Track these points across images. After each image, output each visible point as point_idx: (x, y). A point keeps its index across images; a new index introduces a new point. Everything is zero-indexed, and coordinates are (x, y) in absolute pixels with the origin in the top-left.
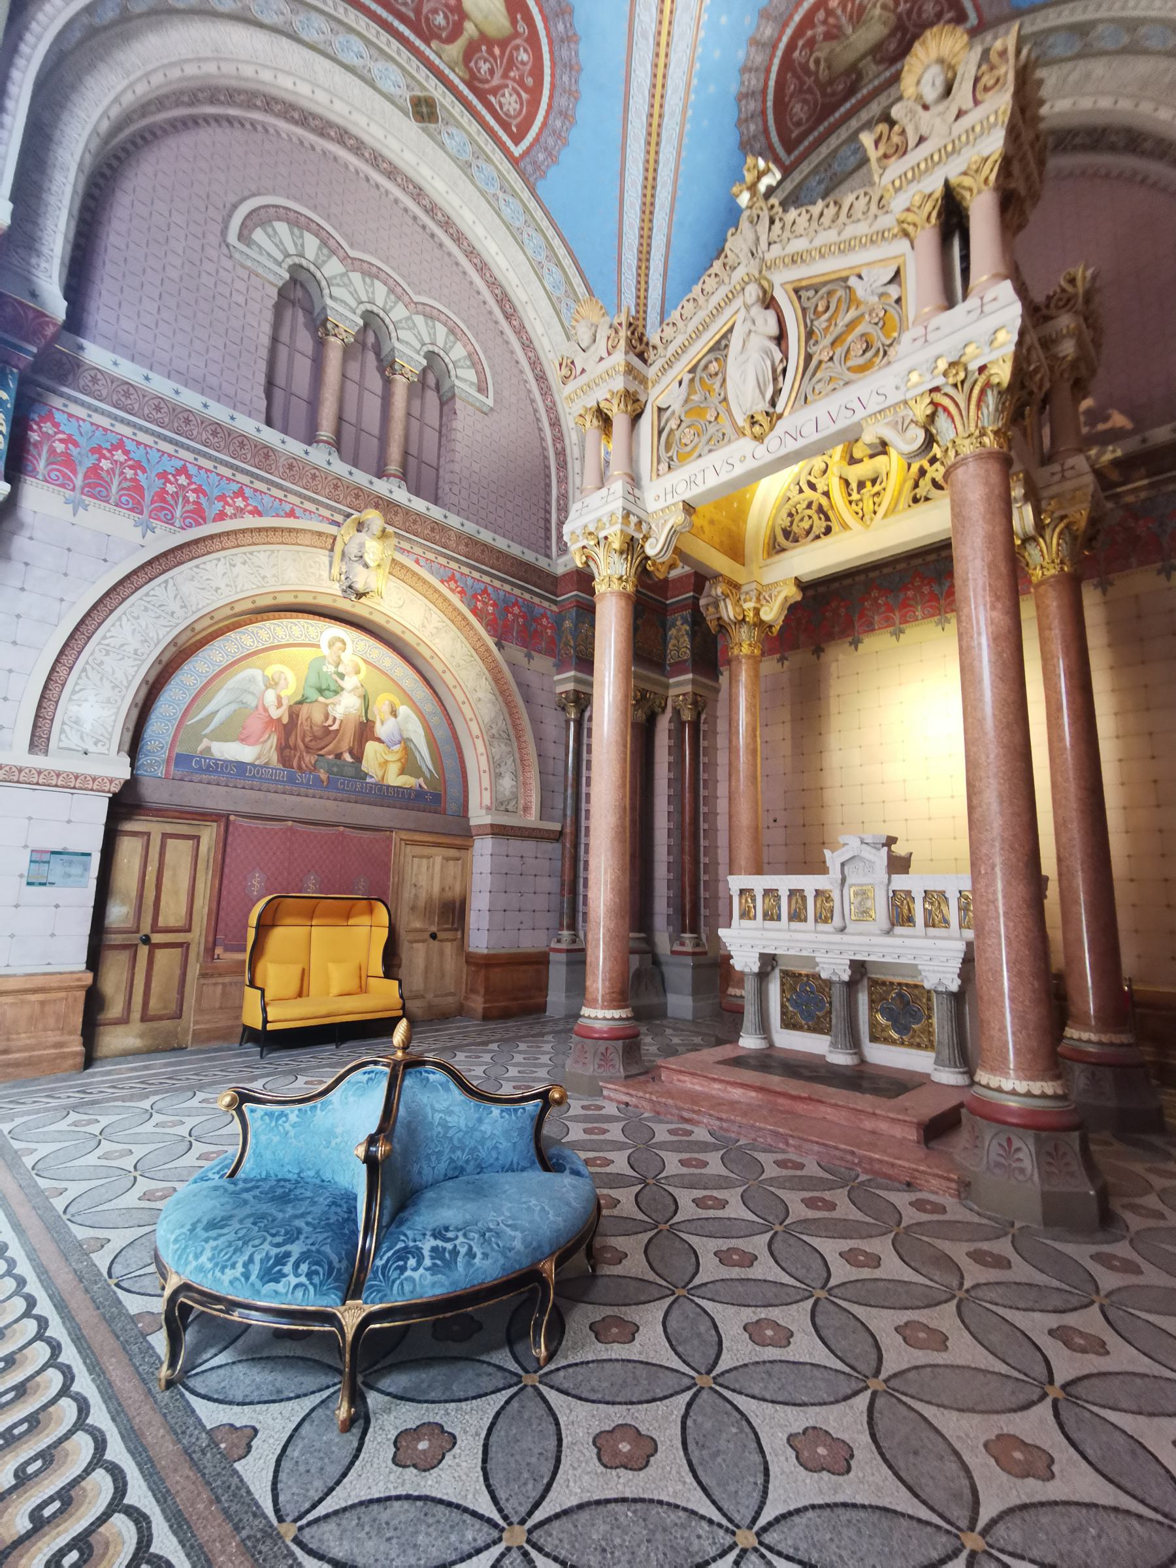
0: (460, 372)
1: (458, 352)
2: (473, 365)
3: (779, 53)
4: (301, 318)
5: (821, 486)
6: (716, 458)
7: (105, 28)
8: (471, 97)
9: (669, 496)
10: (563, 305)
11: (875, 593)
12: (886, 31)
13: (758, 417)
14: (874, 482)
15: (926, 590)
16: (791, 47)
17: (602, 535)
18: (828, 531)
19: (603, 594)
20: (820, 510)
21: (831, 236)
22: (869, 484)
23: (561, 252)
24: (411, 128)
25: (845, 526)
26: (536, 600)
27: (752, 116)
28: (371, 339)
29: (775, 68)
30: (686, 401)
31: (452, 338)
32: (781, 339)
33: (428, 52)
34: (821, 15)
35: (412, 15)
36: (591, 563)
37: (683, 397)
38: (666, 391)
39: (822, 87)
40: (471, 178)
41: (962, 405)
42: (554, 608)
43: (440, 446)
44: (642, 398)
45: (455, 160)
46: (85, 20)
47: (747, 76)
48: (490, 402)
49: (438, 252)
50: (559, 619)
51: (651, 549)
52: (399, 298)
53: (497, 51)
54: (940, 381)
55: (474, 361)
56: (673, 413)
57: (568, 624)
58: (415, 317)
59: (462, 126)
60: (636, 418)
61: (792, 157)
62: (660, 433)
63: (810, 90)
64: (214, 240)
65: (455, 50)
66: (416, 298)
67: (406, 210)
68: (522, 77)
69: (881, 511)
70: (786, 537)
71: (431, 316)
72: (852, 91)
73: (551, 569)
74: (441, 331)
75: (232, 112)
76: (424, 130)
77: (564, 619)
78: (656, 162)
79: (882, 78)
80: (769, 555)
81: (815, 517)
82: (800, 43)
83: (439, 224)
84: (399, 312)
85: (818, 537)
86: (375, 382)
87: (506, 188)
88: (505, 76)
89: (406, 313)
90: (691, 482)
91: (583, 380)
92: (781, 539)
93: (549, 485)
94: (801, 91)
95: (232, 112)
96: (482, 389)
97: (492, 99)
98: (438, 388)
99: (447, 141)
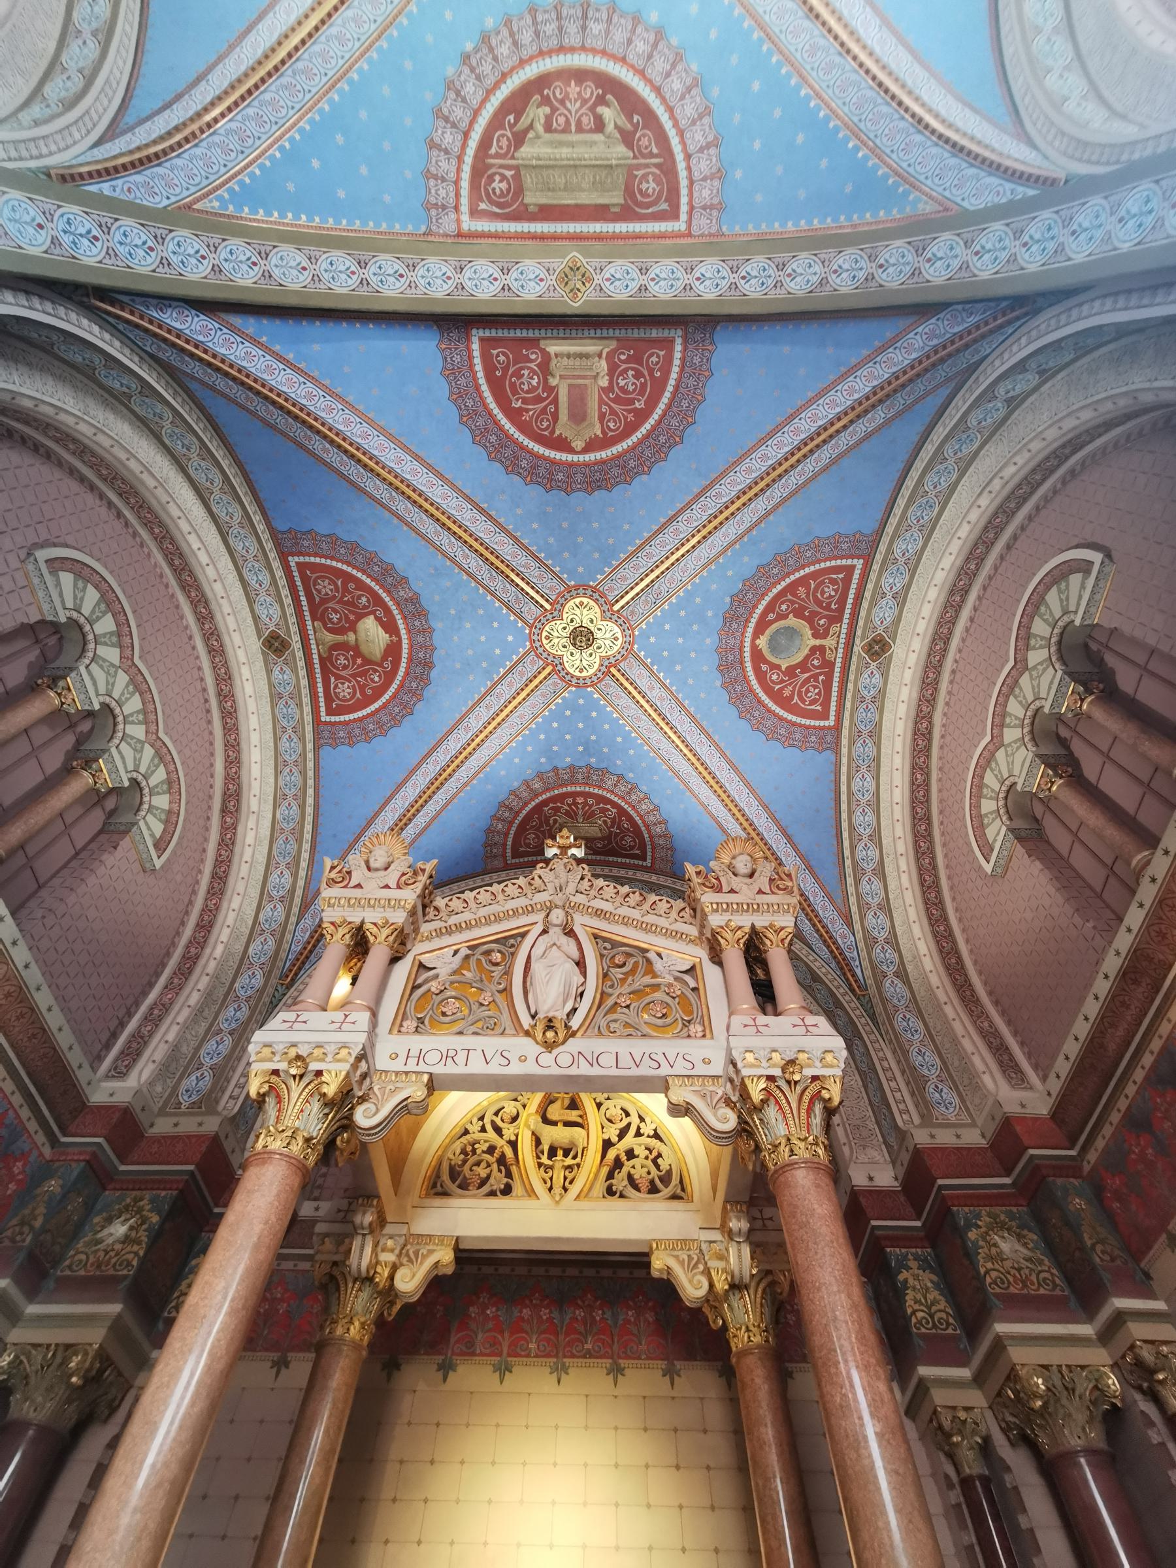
0: (150, 818)
1: (162, 801)
4: (33, 655)
5: (509, 1132)
6: (491, 1043)
7: (101, 386)
9: (412, 1062)
10: (283, 837)
11: (484, 1297)
13: (557, 1024)
14: (566, 1153)
15: (544, 1313)
16: (545, 803)
17: (314, 1066)
18: (507, 1191)
19: (267, 1154)
20: (502, 1160)
21: (635, 914)
22: (560, 1152)
23: (310, 801)
24: (255, 645)
25: (531, 1193)
26: (32, 1126)
28: (85, 726)
30: (454, 973)
31: (165, 787)
32: (581, 964)
34: (570, 800)
36: (271, 1101)
37: (455, 966)
38: (439, 952)
40: (273, 706)
41: (794, 1105)
42: (47, 1151)
43: (65, 866)
44: (409, 946)
45: (271, 686)
46: (97, 360)
48: (158, 863)
49: (204, 724)
50: (45, 1171)
51: (364, 1117)
53: (359, 661)
54: (777, 1072)
55: (170, 819)
56: (437, 976)
57: (53, 1185)
58: (147, 746)
59: (294, 675)
60: (395, 960)
62: (415, 988)
64: (32, 538)
65: (330, 638)
66: (161, 734)
68: (365, 686)
69: (574, 1190)
70: (451, 1178)
71: (162, 756)
73: (87, 1090)
74: (160, 775)
75: (127, 513)
76: (263, 652)
77: (50, 1176)
80: (427, 1195)
81: (495, 1166)
83: (222, 710)
85: (492, 1194)
86: (53, 760)
87: (298, 729)
88: (354, 676)
89: (142, 737)
90: (447, 1056)
91: (349, 893)
92: (445, 1177)
93: (151, 985)
95: (127, 513)
98: (111, 814)
99: (276, 671)
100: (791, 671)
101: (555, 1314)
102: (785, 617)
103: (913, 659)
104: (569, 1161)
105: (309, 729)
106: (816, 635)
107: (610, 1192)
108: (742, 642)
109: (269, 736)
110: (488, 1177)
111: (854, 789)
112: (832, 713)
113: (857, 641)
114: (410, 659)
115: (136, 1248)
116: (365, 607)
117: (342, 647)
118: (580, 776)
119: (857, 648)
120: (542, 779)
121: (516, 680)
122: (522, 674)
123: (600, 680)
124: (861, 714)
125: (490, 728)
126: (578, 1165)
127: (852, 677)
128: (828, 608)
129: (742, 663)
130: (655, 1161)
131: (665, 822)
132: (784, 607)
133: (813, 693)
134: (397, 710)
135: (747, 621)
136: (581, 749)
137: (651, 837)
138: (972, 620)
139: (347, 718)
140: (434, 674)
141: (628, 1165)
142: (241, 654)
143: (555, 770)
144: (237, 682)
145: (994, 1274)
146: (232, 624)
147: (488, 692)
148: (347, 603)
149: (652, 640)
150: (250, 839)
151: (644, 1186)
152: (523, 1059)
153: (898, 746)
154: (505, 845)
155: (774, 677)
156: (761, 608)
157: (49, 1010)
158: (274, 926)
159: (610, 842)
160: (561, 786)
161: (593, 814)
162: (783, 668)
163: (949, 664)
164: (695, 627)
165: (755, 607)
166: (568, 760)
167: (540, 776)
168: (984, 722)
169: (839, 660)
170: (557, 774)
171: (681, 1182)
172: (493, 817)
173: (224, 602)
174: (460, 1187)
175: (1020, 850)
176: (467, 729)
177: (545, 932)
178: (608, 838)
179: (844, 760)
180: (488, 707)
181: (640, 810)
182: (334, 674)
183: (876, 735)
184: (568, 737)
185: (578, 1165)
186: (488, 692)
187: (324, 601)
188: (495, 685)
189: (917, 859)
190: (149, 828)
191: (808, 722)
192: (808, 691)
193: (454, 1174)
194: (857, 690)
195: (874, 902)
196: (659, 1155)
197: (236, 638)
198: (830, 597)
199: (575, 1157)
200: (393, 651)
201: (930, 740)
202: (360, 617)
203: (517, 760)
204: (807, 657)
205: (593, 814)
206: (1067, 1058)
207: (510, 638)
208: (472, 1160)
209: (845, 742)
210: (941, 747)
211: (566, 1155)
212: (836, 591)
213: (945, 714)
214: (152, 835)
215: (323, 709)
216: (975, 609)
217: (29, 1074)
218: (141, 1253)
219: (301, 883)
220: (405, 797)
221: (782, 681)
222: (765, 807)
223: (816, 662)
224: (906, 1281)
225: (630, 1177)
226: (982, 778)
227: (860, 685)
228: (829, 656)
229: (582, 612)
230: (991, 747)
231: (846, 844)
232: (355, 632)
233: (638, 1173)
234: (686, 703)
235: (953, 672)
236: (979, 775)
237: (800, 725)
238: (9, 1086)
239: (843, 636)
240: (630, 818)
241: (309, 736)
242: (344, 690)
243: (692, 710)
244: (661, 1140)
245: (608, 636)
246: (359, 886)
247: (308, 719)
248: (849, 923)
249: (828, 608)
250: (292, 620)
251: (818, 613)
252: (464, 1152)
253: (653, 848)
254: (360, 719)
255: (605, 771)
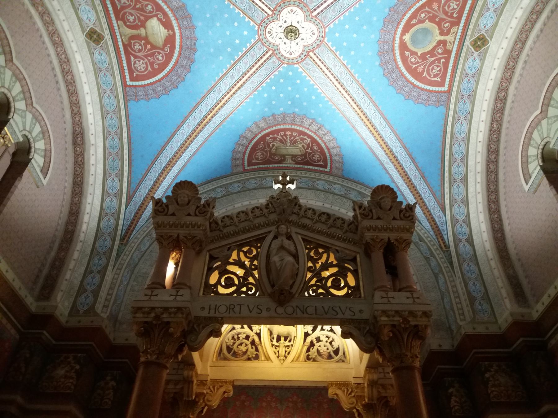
2: (45, 157)
3: (263, 134)
8: (122, 52)
9: (212, 311)
12: (300, 153)
15: (273, 405)
16: (267, 135)
18: (257, 357)
20: (253, 343)
22: (282, 339)
23: (125, 135)
24: (82, 38)
25: (268, 359)
26: (9, 326)
27: (242, 145)
29: (258, 137)
31: (41, 135)
33: (115, 24)
34: (282, 133)
35: (119, 7)
39: (271, 154)
40: (97, 76)
47: (248, 132)
52: (25, 99)
53: (149, 47)
58: (28, 113)
59: (107, 55)
61: (249, 168)
63: (266, 152)
67: (51, 62)
69: (291, 357)
71: (37, 118)
72: (280, 162)
74: (37, 129)
76: (87, 42)
78: (198, 133)
79: (291, 166)
81: (250, 346)
82: (271, 136)
83: (66, 81)
84: (20, 105)
85: (249, 359)
88: (146, 56)
92: (225, 351)
94: (263, 150)
96: (45, 171)
97: (132, 58)
99: (96, 54)
100: (423, 57)
101: (279, 405)
102: (423, 22)
103: (501, 53)
104: (287, 343)
105: (120, 90)
106: (442, 33)
107: (308, 358)
108: (394, 37)
109: (96, 96)
110: (247, 350)
111: (455, 130)
112: (447, 82)
113: (468, 38)
114: (181, 46)
115: (71, 381)
116: (150, 12)
117: (137, 37)
118: (289, 119)
119: (468, 42)
120: (265, 121)
121: (249, 60)
122: (253, 56)
123: (303, 60)
124: (465, 84)
125: (233, 90)
126: (292, 345)
127: (461, 61)
128: (451, 16)
129: (393, 50)
130: (331, 343)
131: (339, 147)
132: (423, 15)
133: (436, 70)
134: (174, 78)
135: (399, 24)
136: (289, 103)
137: (331, 156)
138: (541, 31)
139: (143, 83)
140: (197, 55)
141: (317, 345)
142: (74, 45)
143: (274, 115)
144: (73, 64)
145: (495, 393)
146: (66, 27)
147: (232, 67)
148: (138, 9)
149: (337, 35)
150: (92, 161)
151: (326, 355)
152: (268, 309)
153: (485, 107)
154: (243, 159)
155: (413, 60)
156: (408, 15)
157: (7, 271)
158: (113, 211)
159: (306, 158)
160: (277, 125)
161: (296, 142)
162: (419, 55)
163: (523, 57)
164: (365, 27)
165: (404, 15)
166: (282, 109)
167: (264, 119)
168: (538, 99)
169: (455, 49)
170: (275, 118)
171: (344, 354)
172: (237, 143)
173: (60, 13)
174: (232, 355)
175: (545, 181)
176: (219, 91)
177: (276, 237)
178: (305, 155)
179: (451, 112)
180: (232, 77)
181: (325, 140)
182: (133, 55)
183: (472, 98)
184: (281, 95)
185: (292, 345)
186: (232, 67)
187: (123, 8)
188: (236, 63)
189: (488, 175)
190: (36, 162)
191: (431, 88)
192: (433, 69)
193: (229, 349)
194: (464, 69)
195: (459, 198)
196: (333, 340)
197: (70, 35)
198: (454, 9)
199: (290, 341)
200: (170, 40)
201: (505, 104)
202: (148, 18)
203: (250, 110)
204: (435, 47)
205: (296, 142)
206: (549, 296)
207: (245, 33)
208: (238, 342)
209: (453, 101)
210: (511, 108)
211: (285, 340)
212: (458, 5)
213: (516, 88)
214: (39, 166)
215: (127, 77)
216: (545, 24)
217: (15, 318)
218: (75, 383)
219: (125, 185)
220: (183, 134)
221: (418, 62)
222: (400, 141)
223: (440, 51)
224: (452, 392)
225: (318, 351)
226: (532, 134)
227: (466, 66)
228: (449, 46)
229: (292, 16)
230: (539, 117)
231: (447, 163)
232: (145, 28)
233: (323, 349)
234: (356, 76)
235: (525, 62)
236: (530, 133)
237: (426, 90)
238: (4, 321)
239: (459, 34)
240: (318, 144)
241: (121, 95)
242: (140, 65)
243: (360, 80)
244: (334, 333)
245: (308, 32)
246: (173, 214)
247: (119, 84)
248: (443, 210)
249: (451, 16)
250: (103, 20)
251: (444, 19)
252: (233, 338)
253: (332, 162)
254: (152, 84)
255: (304, 117)
